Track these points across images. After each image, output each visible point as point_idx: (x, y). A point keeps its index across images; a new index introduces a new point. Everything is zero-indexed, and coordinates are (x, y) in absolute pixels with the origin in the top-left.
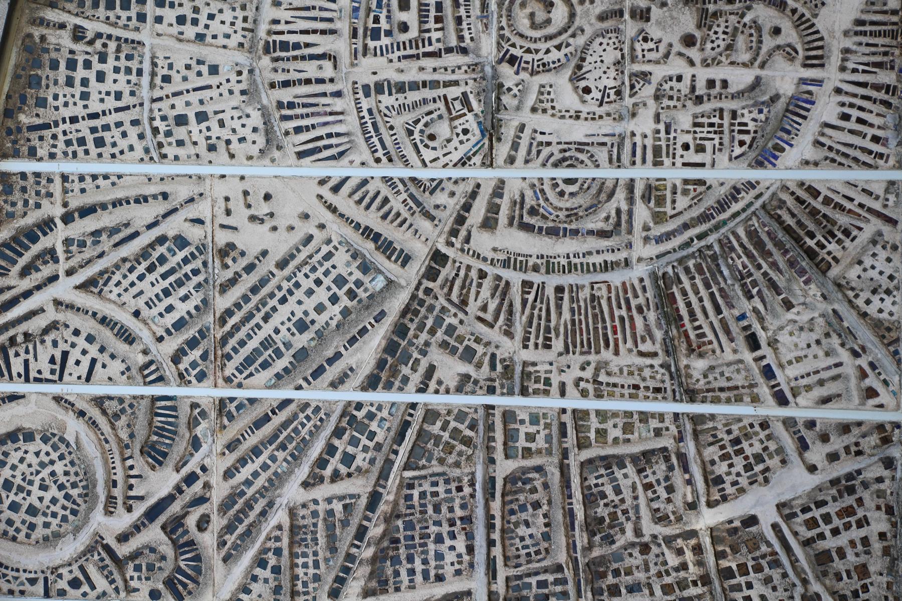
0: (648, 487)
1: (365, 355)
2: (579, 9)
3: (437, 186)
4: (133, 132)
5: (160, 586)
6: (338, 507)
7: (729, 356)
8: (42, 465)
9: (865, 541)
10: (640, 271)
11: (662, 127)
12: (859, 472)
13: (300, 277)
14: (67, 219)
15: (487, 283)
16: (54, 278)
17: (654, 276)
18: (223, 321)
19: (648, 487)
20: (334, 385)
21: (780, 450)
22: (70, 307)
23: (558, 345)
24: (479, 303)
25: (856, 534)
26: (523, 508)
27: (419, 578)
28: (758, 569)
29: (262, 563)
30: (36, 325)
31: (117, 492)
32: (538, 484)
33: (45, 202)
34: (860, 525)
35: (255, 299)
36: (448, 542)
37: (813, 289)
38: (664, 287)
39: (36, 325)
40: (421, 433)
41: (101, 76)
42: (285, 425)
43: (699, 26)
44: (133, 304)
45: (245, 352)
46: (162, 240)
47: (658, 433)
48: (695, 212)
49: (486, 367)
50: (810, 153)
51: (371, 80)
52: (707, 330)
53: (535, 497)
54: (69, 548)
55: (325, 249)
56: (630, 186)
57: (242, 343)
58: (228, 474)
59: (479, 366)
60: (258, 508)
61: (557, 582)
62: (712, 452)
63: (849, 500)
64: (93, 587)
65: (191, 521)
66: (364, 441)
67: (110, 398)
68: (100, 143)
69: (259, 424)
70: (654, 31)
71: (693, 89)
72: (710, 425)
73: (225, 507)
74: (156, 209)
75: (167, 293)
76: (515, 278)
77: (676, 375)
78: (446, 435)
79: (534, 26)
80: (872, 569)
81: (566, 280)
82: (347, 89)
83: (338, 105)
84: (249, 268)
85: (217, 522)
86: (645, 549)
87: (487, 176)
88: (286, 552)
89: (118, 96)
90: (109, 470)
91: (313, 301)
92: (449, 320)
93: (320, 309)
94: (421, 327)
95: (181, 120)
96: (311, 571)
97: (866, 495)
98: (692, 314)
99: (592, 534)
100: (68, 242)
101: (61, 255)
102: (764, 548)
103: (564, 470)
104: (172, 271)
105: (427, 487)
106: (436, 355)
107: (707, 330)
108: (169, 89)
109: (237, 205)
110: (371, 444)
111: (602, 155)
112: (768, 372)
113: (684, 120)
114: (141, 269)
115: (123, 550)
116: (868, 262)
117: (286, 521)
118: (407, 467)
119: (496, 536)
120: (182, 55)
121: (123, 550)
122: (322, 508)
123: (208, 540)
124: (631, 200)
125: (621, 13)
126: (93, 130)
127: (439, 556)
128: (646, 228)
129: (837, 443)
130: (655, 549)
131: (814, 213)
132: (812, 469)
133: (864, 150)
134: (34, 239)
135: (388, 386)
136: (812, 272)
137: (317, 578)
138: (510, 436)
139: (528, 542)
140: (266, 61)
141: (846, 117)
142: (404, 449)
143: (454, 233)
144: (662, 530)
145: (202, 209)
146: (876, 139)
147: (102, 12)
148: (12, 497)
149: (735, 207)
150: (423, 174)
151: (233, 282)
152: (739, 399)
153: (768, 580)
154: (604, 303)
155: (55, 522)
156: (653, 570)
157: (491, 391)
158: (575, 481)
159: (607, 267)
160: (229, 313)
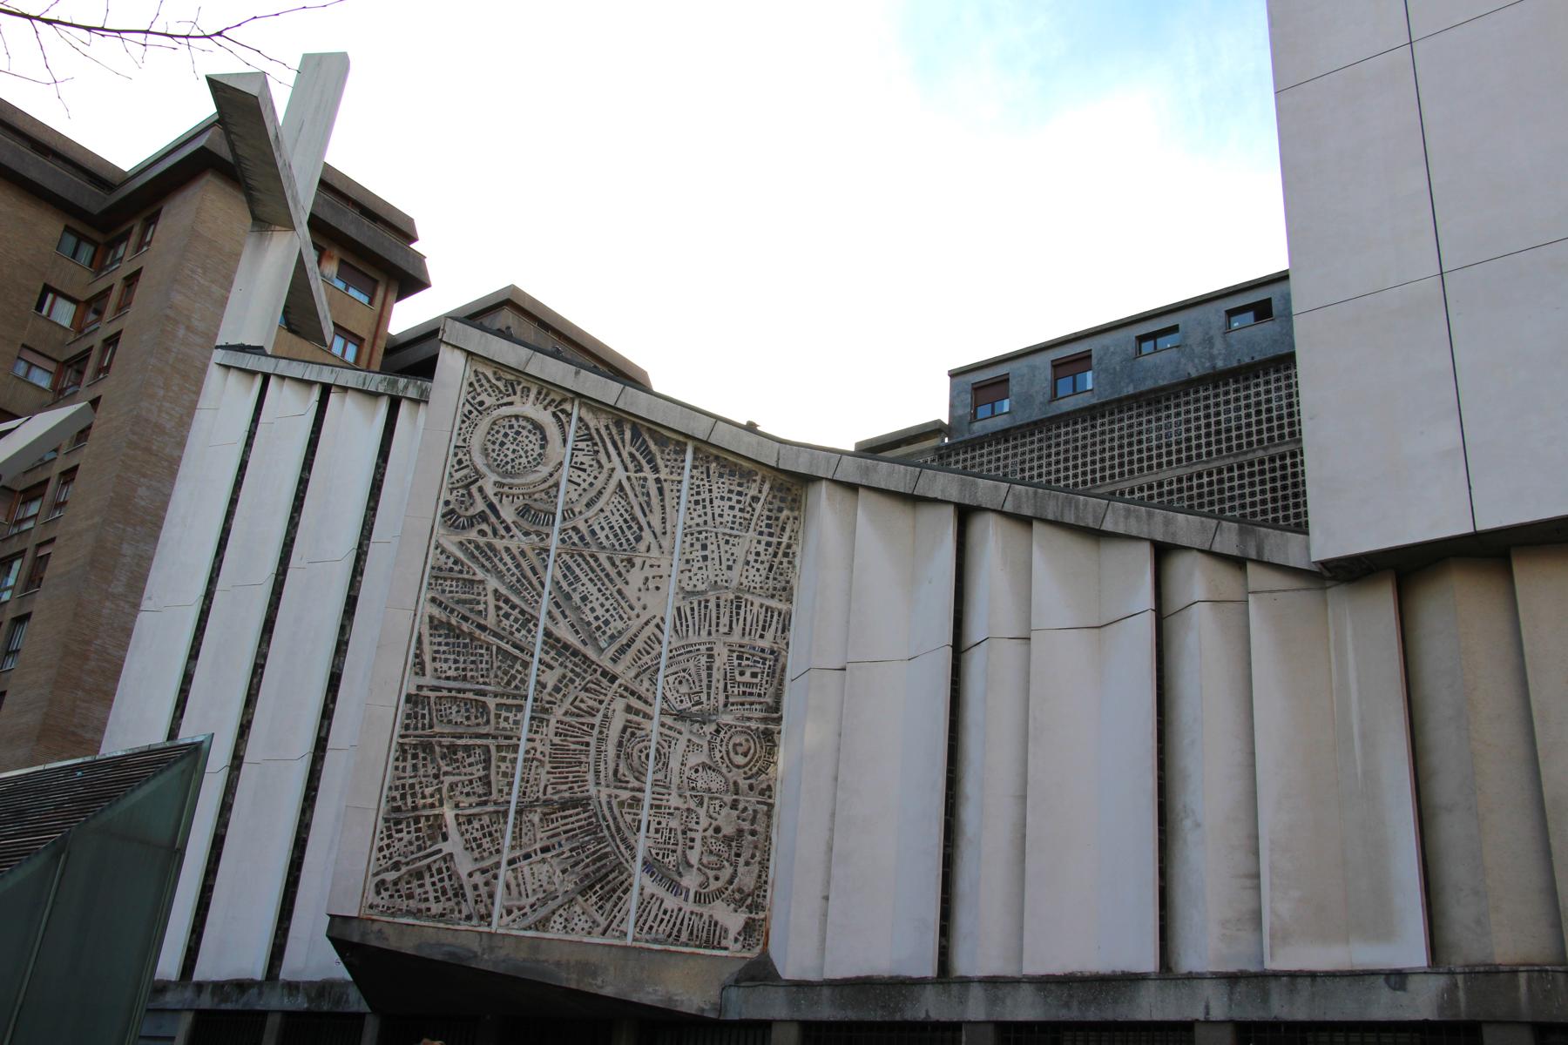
0: (471, 782)
1: (563, 632)
3: (653, 682)
4: (700, 521)
6: (481, 607)
7: (539, 835)
9: (427, 900)
10: (593, 791)
14: (658, 480)
15: (596, 704)
16: (626, 470)
17: (589, 798)
18: (592, 556)
19: (471, 782)
20: (549, 613)
21: (482, 858)
23: (557, 740)
25: (431, 895)
28: (418, 838)
29: (455, 563)
30: (602, 457)
31: (506, 489)
35: (602, 575)
37: (571, 886)
38: (582, 803)
39: (602, 457)
40: (516, 658)
41: (732, 508)
42: (530, 583)
44: (607, 510)
45: (574, 566)
46: (641, 529)
47: (501, 791)
48: (622, 825)
50: (647, 891)
51: (715, 652)
54: (479, 461)
56: (641, 790)
58: (507, 549)
60: (487, 564)
62: (486, 820)
63: (450, 893)
65: (484, 527)
68: (697, 503)
69: (533, 569)
70: (725, 811)
74: (658, 528)
76: (597, 720)
77: (531, 805)
82: (712, 639)
83: (704, 633)
84: (619, 574)
85: (482, 541)
86: (436, 776)
87: (655, 711)
89: (721, 516)
90: (518, 486)
91: (597, 606)
92: (578, 681)
93: (593, 610)
94: (576, 665)
95: (704, 547)
97: (452, 903)
99: (448, 747)
100: (645, 479)
103: (486, 736)
105: (486, 658)
106: (559, 671)
108: (722, 543)
109: (655, 571)
111: (660, 776)
112: (527, 856)
113: (674, 824)
114: (626, 516)
115: (474, 489)
116: (583, 918)
117: (477, 578)
118: (499, 648)
119: (454, 694)
120: (739, 552)
121: (474, 489)
122: (482, 598)
123: (473, 534)
124: (633, 789)
127: (446, 661)
129: (483, 890)
131: (614, 891)
132: (470, 875)
134: (649, 462)
135: (545, 643)
136: (581, 886)
137: (443, 591)
138: (508, 708)
140: (732, 596)
141: (665, 912)
142: (508, 647)
143: (626, 689)
145: (655, 552)
146: (651, 928)
147: (766, 513)
149: (622, 848)
151: (613, 564)
152: (514, 838)
153: (411, 843)
157: (535, 700)
158: (479, 742)
159: (597, 772)
160: (596, 560)
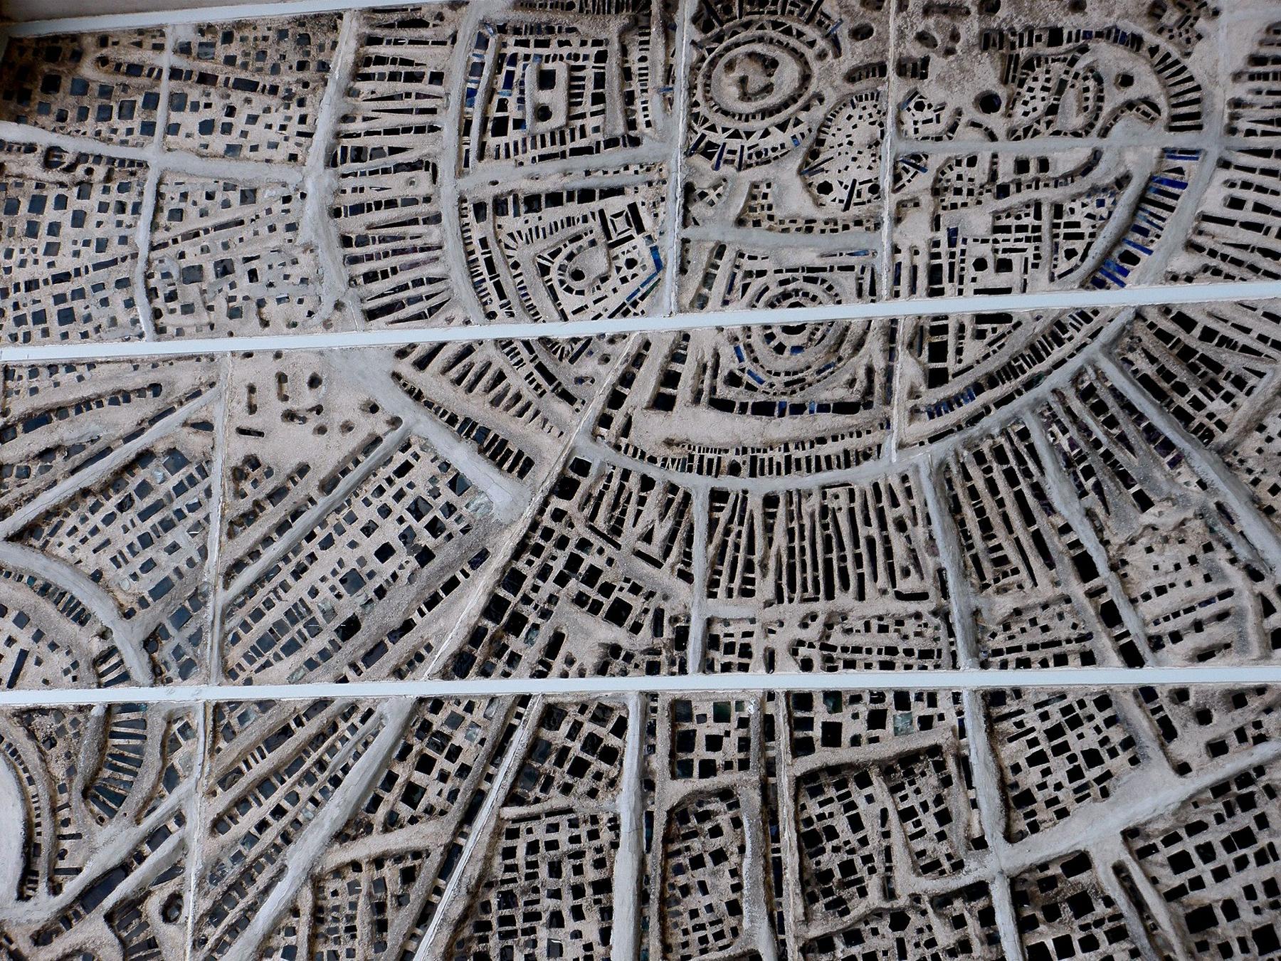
2: (816, 67)
6: (390, 872)
11: (942, 236)
12: (1260, 770)
13: (357, 503)
15: (654, 496)
23: (764, 588)
26: (697, 862)
32: (724, 820)
34: (1262, 858)
36: (571, 924)
43: (1004, 81)
45: (260, 628)
46: (144, 457)
48: (993, 365)
49: (646, 631)
51: (487, 194)
53: (718, 843)
55: (400, 458)
57: (257, 615)
58: (218, 825)
59: (636, 628)
63: (1244, 820)
65: (152, 907)
66: (442, 763)
67: (43, 711)
68: (66, 317)
71: (993, 175)
73: (213, 873)
75: (146, 541)
76: (699, 485)
78: (576, 747)
79: (745, 97)
84: (276, 495)
85: (192, 906)
86: (899, 921)
92: (590, 559)
94: (544, 573)
95: (192, 275)
102: (1100, 909)
107: (1010, 551)
108: (179, 228)
110: (452, 768)
113: (977, 220)
125: (882, 69)
128: (913, 394)
129: (1223, 723)
130: (915, 920)
131: (1186, 354)
135: (485, 673)
138: (683, 741)
139: (704, 918)
141: (1236, 204)
144: (931, 885)
152: (1061, 660)
157: (653, 669)
159: (847, 460)
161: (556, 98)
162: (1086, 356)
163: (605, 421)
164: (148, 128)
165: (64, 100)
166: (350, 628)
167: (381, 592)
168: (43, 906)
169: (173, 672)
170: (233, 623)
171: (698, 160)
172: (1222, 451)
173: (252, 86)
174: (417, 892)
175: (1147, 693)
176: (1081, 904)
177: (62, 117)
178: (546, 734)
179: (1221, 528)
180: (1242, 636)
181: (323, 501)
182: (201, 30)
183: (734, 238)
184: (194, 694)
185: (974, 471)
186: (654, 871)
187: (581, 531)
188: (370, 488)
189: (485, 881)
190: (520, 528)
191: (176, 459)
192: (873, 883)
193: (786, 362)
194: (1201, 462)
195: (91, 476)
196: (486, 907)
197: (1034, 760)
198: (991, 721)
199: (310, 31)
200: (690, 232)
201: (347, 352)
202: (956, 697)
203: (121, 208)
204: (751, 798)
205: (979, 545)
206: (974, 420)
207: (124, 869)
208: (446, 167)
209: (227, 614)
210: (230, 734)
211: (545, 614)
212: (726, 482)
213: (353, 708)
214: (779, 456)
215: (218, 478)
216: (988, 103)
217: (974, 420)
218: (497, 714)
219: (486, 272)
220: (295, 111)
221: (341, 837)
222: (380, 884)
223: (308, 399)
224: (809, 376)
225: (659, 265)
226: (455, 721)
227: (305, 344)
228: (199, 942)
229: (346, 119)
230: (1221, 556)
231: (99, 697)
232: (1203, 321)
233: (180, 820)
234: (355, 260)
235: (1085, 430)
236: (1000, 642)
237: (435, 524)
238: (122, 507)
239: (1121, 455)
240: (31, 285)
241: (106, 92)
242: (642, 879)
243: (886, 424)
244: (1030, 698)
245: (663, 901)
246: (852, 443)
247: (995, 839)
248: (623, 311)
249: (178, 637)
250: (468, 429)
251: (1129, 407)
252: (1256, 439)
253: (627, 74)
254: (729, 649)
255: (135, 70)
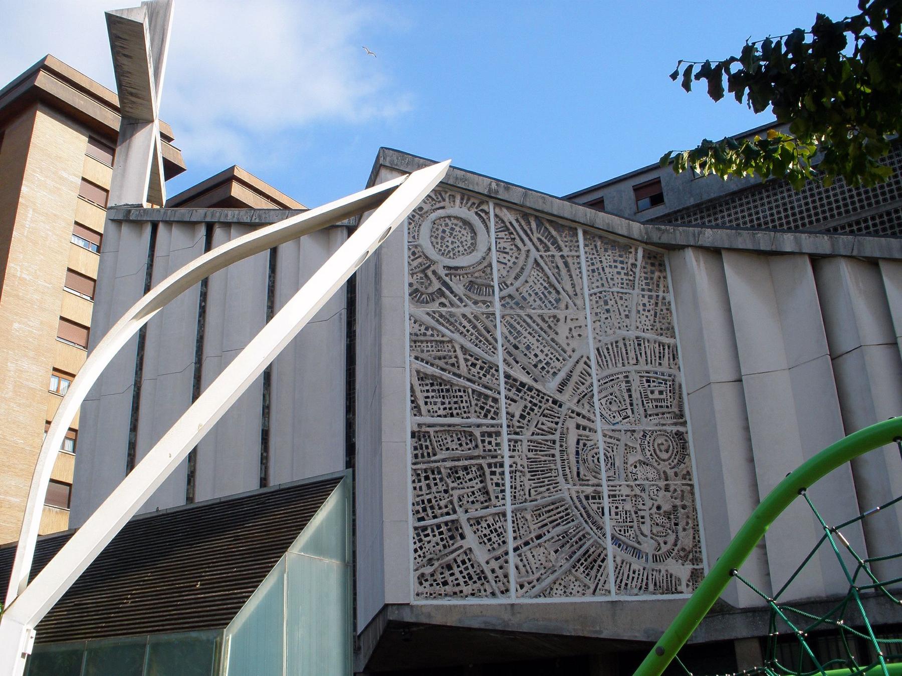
2: (667, 463)
5: (415, 287)
6: (454, 360)
8: (462, 242)
9: (458, 585)
11: (624, 498)
12: (488, 582)
13: (549, 348)
14: (562, 257)
15: (554, 425)
16: (538, 250)
22: (527, 256)
23: (531, 455)
24: (545, 422)
25: (461, 581)
26: (459, 439)
27: (426, 394)
28: (442, 539)
32: (470, 446)
33: (568, 249)
34: (465, 582)
36: (442, 407)
43: (665, 512)
45: (515, 324)
46: (558, 292)
48: (591, 512)
49: (518, 424)
51: (630, 379)
52: (542, 518)
53: (464, 444)
55: (561, 358)
56: (599, 485)
57: (518, 323)
58: (464, 316)
59: (519, 422)
61: (428, 454)
63: (475, 578)
64: (413, 260)
65: (443, 300)
66: (482, 372)
67: (491, 269)
68: (593, 271)
71: (640, 510)
72: (502, 519)
73: (452, 315)
75: (536, 294)
76: (557, 437)
78: (487, 407)
79: (659, 445)
80: (447, 587)
81: (558, 457)
84: (550, 327)
85: (443, 310)
86: (446, 491)
88: (433, 339)
92: (536, 409)
94: (532, 397)
95: (606, 303)
96: (425, 349)
98: (549, 511)
101: (548, 253)
102: (451, 542)
103: (477, 457)
104: (545, 296)
107: (542, 518)
108: (618, 299)
110: (481, 375)
113: (628, 506)
115: (430, 273)
116: (577, 583)
118: (473, 391)
125: (667, 480)
126: (598, 269)
127: (435, 403)
128: (583, 492)
129: (500, 572)
130: (446, 496)
131: (595, 561)
133: (621, 580)
134: (553, 244)
135: (506, 383)
137: (422, 351)
138: (490, 435)
139: (445, 441)
141: (634, 572)
144: (455, 500)
146: (626, 584)
148: (448, 231)
150: (596, 399)
152: (514, 531)
154: (549, 475)
155: (439, 246)
156: (437, 495)
157: (508, 426)
159: (565, 475)
161: (656, 395)
162: (593, 535)
163: (573, 412)
164: (643, 290)
165: (649, 268)
166: (516, 347)
167: (526, 355)
168: (442, 272)
169: (503, 302)
170: (516, 317)
171: (642, 433)
172: (570, 571)
173: (655, 316)
174: (449, 367)
175: (507, 553)
176: (452, 537)
177: (644, 268)
178: (490, 399)
179: (550, 571)
180: (522, 577)
181: (549, 339)
182: (669, 303)
183: (621, 444)
184: (497, 308)
185: (563, 508)
186: (457, 428)
187: (544, 406)
188: (553, 351)
189: (452, 385)
190: (544, 391)
191: (558, 301)
192: (455, 485)
193: (590, 458)
194: (567, 566)
195: (553, 279)
196: (446, 385)
197: (489, 526)
198: (498, 514)
199: (670, 330)
200: (623, 432)
201: (588, 343)
202: (504, 505)
203: (622, 284)
204: (476, 453)
205: (544, 510)
206: (576, 507)
207: (452, 292)
208: (637, 368)
209: (518, 315)
210: (487, 318)
211: (521, 398)
212: (558, 444)
213: (495, 349)
214: (565, 457)
215: (554, 312)
216: (659, 508)
217: (576, 507)
218: (495, 386)
219: (610, 379)
220: (649, 328)
221: (462, 347)
222: (450, 358)
223: (575, 334)
224: (586, 464)
225: (614, 424)
226: (493, 375)
227: (590, 333)
228: (434, 312)
229: (648, 341)
230: (543, 571)
231: (496, 284)
232: (603, 565)
233: (465, 306)
234: (612, 345)
235: (575, 536)
236: (519, 516)
237: (543, 368)
238: (545, 287)
239: (568, 545)
240: (601, 262)
241: (652, 279)
242: (454, 425)
243: (574, 485)
244: (504, 524)
245: (449, 431)
246: (569, 476)
247: (468, 515)
248: (602, 415)
249: (512, 303)
250: (569, 376)
251: (581, 547)
252: (573, 579)
253: (663, 414)
254: (514, 446)
255: (658, 286)
